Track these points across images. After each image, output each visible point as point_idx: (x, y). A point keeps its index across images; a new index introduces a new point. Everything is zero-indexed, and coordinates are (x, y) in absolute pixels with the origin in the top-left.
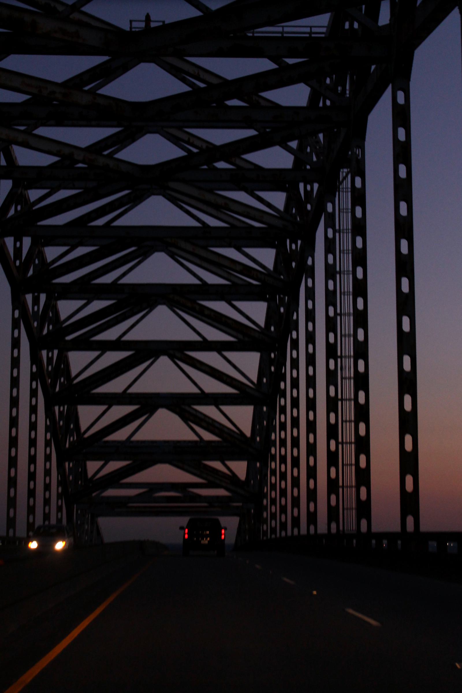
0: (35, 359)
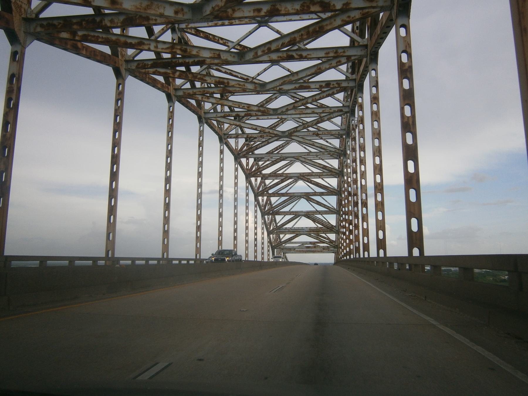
0: (256, 200)
